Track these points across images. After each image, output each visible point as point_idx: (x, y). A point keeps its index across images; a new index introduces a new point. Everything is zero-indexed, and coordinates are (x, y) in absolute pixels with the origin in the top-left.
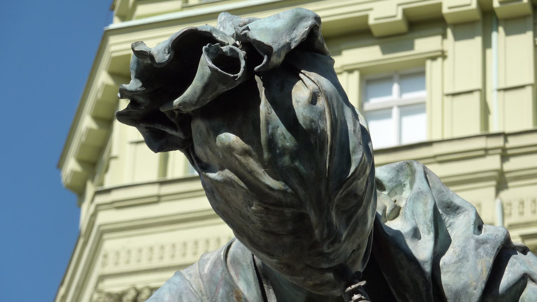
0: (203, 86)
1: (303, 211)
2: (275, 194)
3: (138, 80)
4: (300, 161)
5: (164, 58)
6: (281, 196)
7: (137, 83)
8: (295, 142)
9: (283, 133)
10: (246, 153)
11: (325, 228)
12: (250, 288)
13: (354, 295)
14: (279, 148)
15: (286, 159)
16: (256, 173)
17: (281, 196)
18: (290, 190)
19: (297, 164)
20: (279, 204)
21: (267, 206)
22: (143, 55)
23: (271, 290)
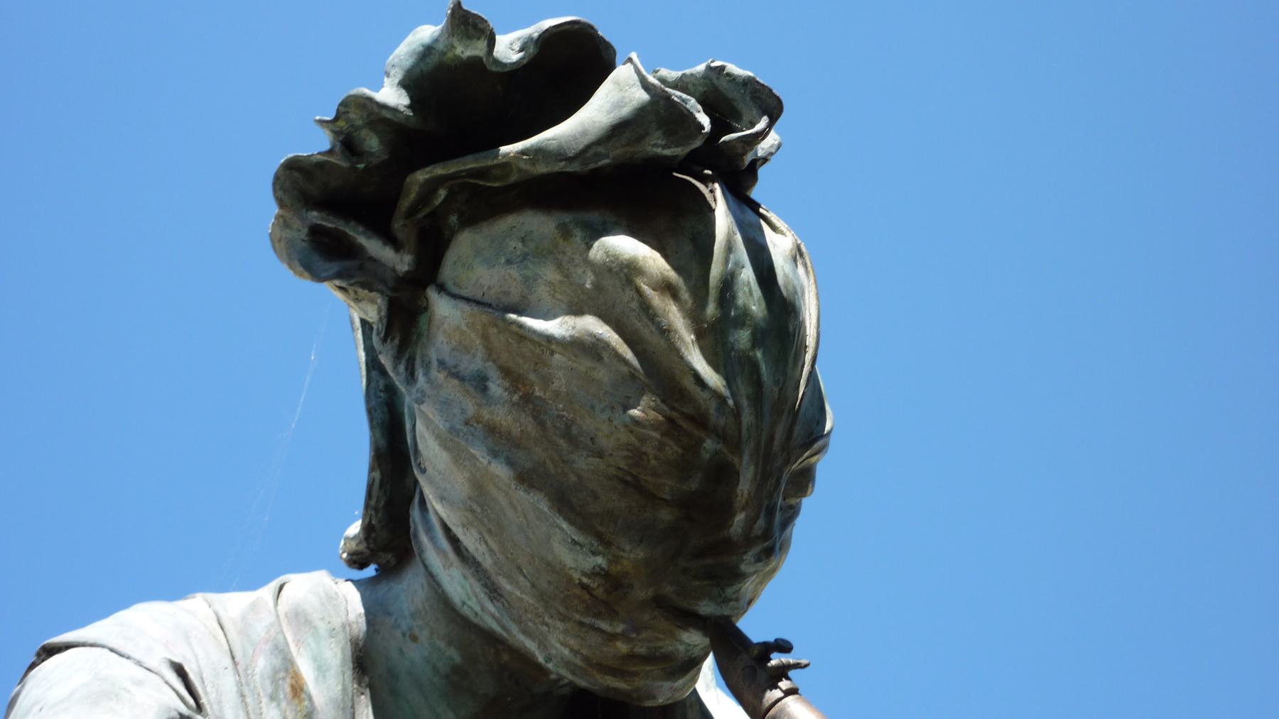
0: (614, 123)
1: (736, 460)
2: (702, 395)
3: (403, 92)
4: (764, 354)
5: (508, 56)
6: (712, 406)
7: (400, 95)
8: (766, 312)
9: (749, 283)
10: (667, 288)
11: (762, 515)
12: (324, 677)
13: (784, 679)
14: (737, 308)
15: (742, 337)
16: (677, 336)
17: (712, 406)
18: (731, 402)
19: (759, 354)
20: (700, 421)
21: (674, 414)
22: (475, 27)
23: (363, 697)
